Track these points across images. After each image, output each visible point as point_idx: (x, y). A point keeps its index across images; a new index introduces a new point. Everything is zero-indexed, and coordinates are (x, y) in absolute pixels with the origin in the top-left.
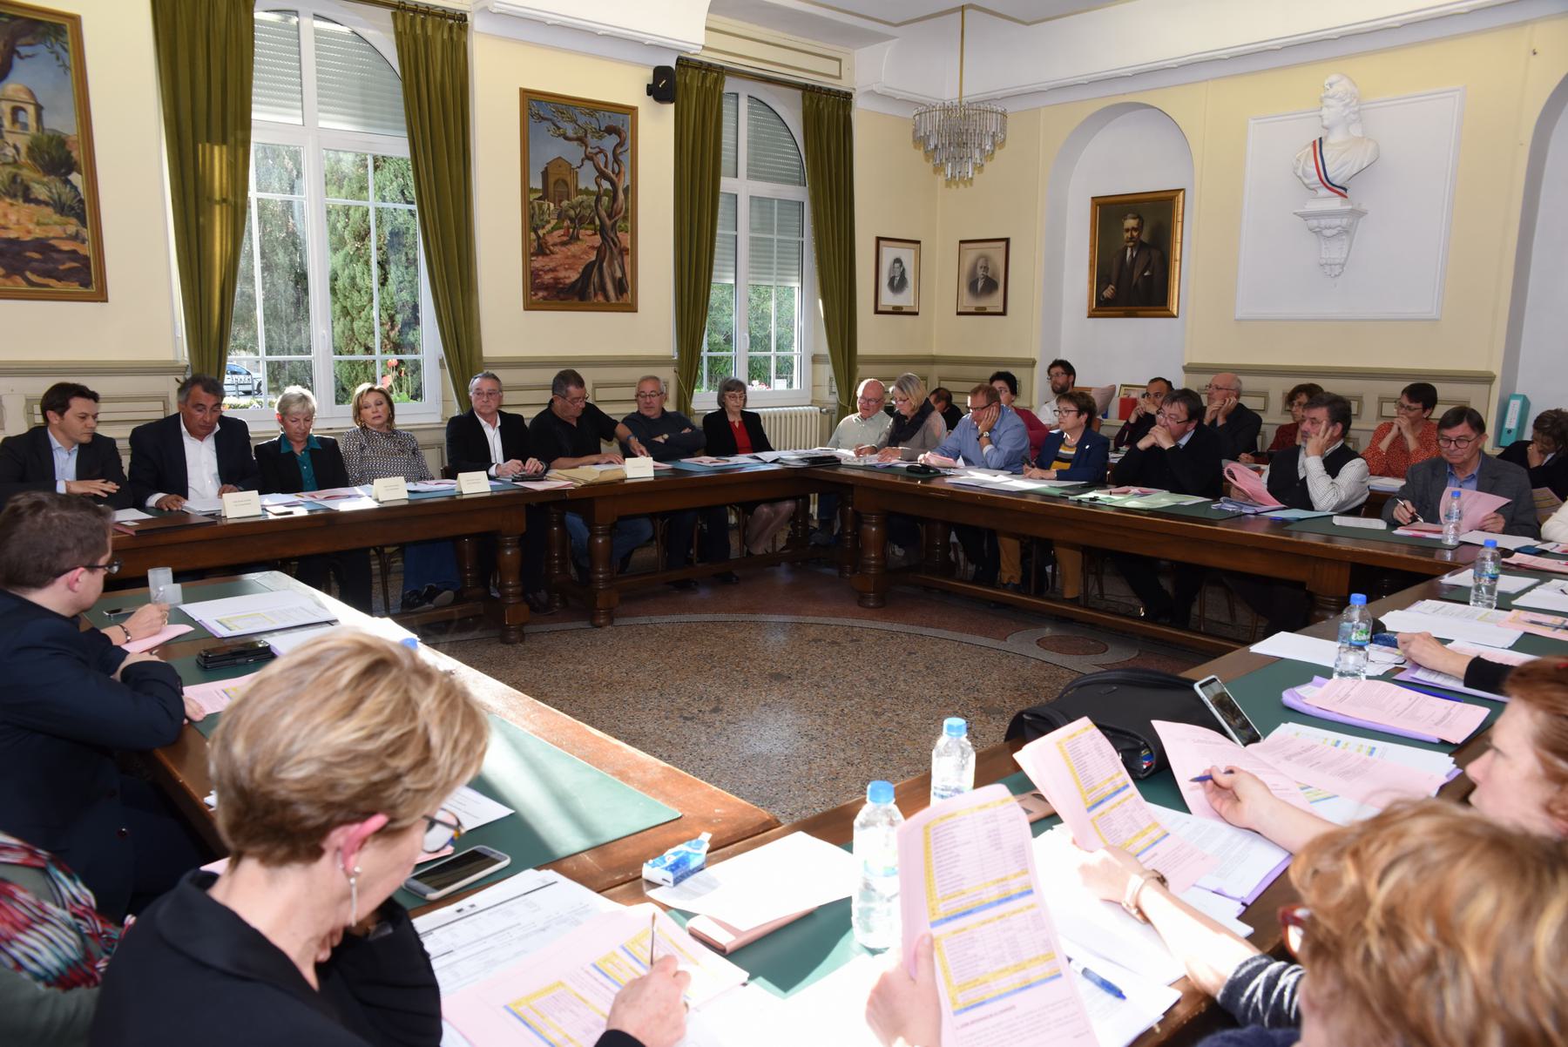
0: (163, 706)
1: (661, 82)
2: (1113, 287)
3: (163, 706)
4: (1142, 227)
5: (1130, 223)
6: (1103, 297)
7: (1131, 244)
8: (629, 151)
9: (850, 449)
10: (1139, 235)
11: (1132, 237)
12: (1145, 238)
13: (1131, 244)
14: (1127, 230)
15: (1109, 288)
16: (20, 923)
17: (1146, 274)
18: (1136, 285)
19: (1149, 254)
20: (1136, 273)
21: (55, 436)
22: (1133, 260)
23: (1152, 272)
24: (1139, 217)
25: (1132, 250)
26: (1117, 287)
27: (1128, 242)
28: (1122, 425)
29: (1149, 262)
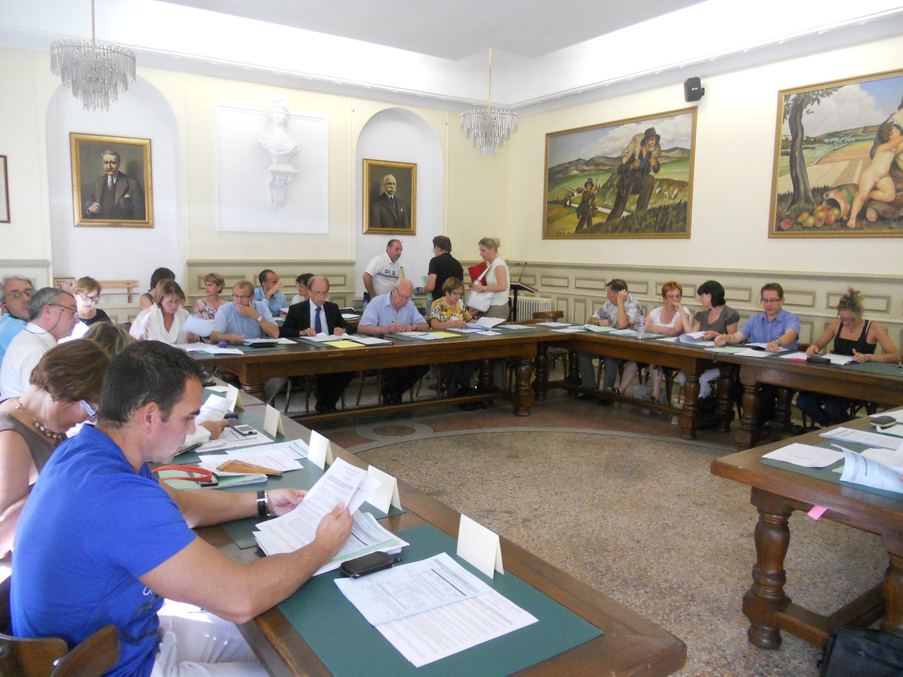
0: (115, 670)
1: (694, 87)
2: (98, 204)
3: (115, 670)
4: (119, 161)
5: (109, 157)
6: (89, 211)
7: (111, 173)
8: (367, 547)
9: (600, 212)
10: (117, 167)
11: (111, 169)
12: (122, 169)
13: (111, 173)
14: (107, 162)
15: (94, 205)
16: (379, 406)
17: (126, 196)
18: (118, 205)
19: (127, 182)
20: (117, 197)
21: (750, 343)
22: (114, 185)
23: (132, 194)
24: (115, 153)
25: (112, 177)
26: (101, 203)
27: (108, 171)
28: (609, 213)
29: (128, 187)
